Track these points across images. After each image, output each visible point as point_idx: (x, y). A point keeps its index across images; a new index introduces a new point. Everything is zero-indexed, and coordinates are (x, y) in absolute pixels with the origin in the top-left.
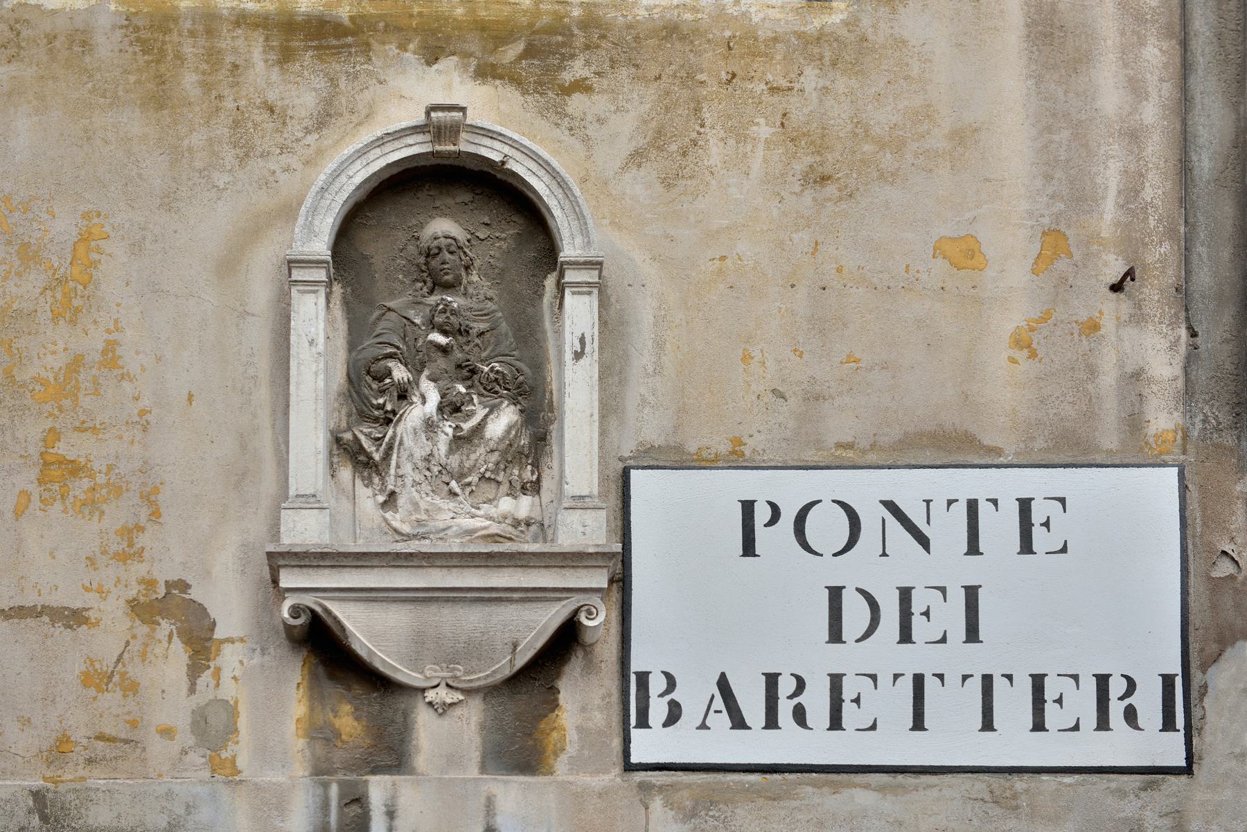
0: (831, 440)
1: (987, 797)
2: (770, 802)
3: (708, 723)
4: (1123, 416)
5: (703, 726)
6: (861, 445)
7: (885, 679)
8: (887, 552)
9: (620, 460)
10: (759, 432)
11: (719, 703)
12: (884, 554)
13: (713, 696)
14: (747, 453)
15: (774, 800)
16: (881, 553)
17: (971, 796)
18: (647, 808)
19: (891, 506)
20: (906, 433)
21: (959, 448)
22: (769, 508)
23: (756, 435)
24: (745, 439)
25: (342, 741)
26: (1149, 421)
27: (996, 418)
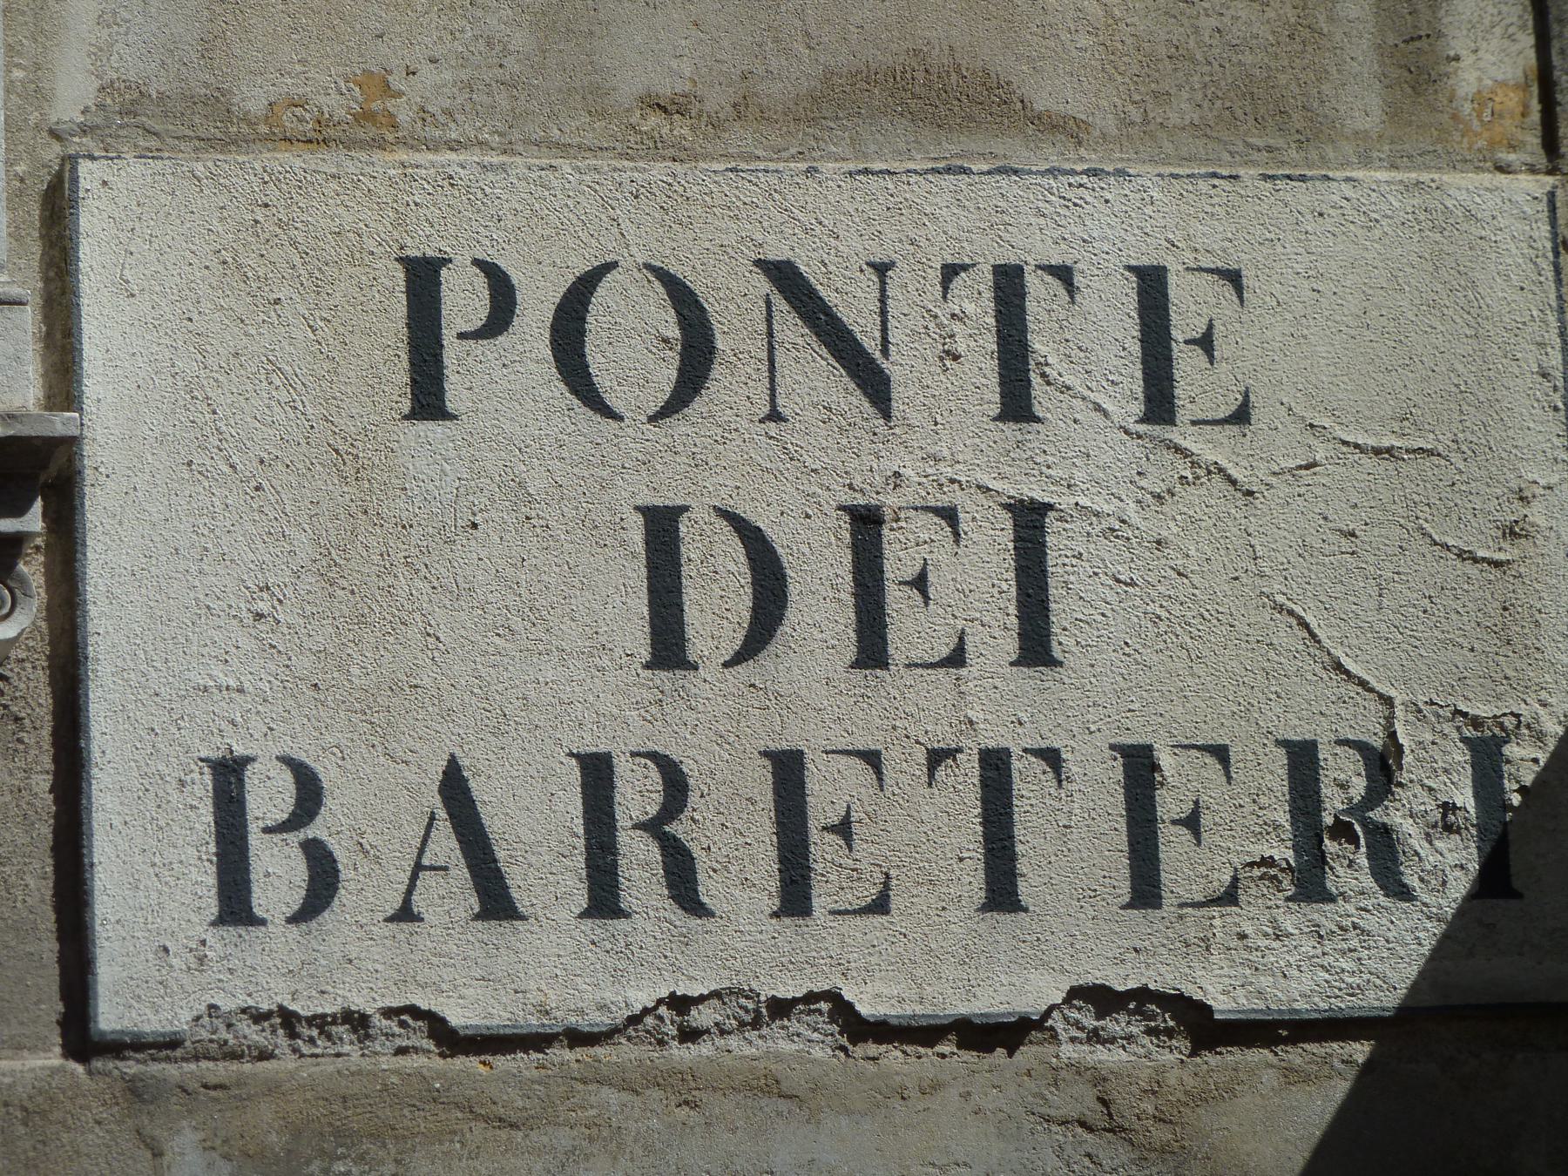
0: (629, 86)
1: (1096, 1115)
2: (503, 1134)
3: (419, 903)
4: (1391, 42)
5: (406, 914)
6: (710, 106)
7: (904, 766)
8: (785, 409)
9: (55, 134)
10: (433, 61)
11: (445, 846)
12: (775, 416)
13: (432, 818)
14: (403, 117)
15: (513, 1126)
16: (766, 410)
17: (1053, 1112)
18: (157, 1154)
19: (784, 277)
20: (829, 74)
21: (971, 118)
22: (481, 282)
23: (426, 70)
24: (396, 81)
25: (1162, 776)
26: (1457, 58)
27: (1065, 36)
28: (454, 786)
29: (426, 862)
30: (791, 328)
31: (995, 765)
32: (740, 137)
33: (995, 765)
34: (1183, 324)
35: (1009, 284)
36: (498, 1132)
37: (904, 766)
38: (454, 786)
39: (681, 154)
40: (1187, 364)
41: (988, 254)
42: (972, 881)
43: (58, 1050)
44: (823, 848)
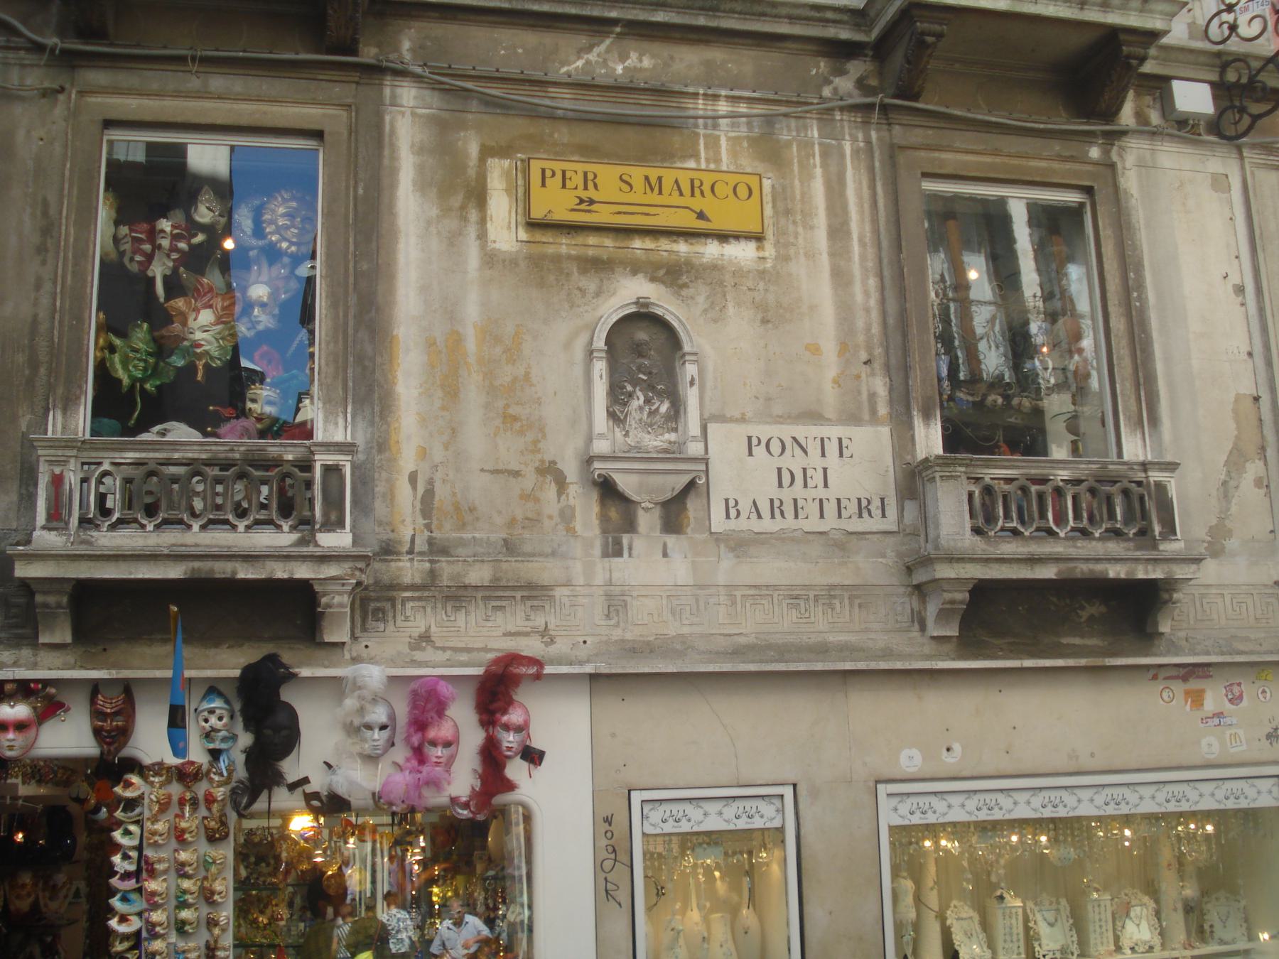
7: (810, 500)
11: (753, 510)
19: (794, 438)
28: (754, 502)
29: (705, 417)
30: (795, 444)
31: (821, 501)
32: (789, 421)
33: (821, 501)
34: (799, 506)
35: (822, 440)
36: (230, 875)
37: (810, 500)
38: (754, 502)
39: (782, 423)
40: (845, 450)
41: (820, 436)
42: (818, 515)
43: (658, 530)
44: (800, 510)
